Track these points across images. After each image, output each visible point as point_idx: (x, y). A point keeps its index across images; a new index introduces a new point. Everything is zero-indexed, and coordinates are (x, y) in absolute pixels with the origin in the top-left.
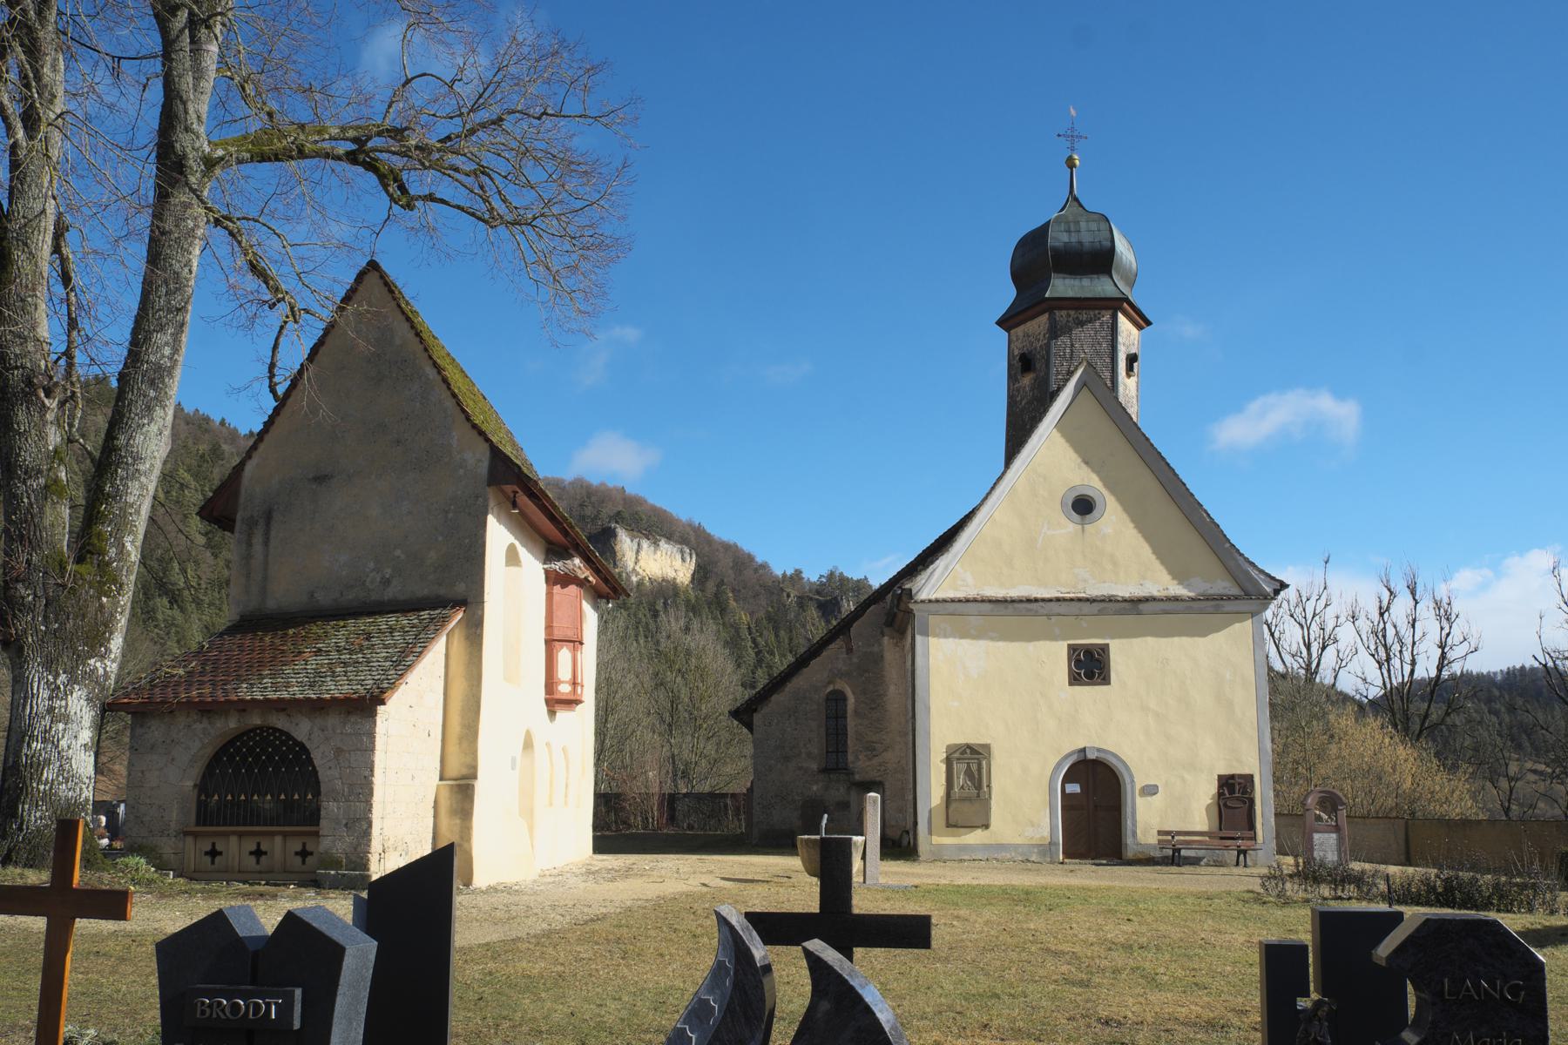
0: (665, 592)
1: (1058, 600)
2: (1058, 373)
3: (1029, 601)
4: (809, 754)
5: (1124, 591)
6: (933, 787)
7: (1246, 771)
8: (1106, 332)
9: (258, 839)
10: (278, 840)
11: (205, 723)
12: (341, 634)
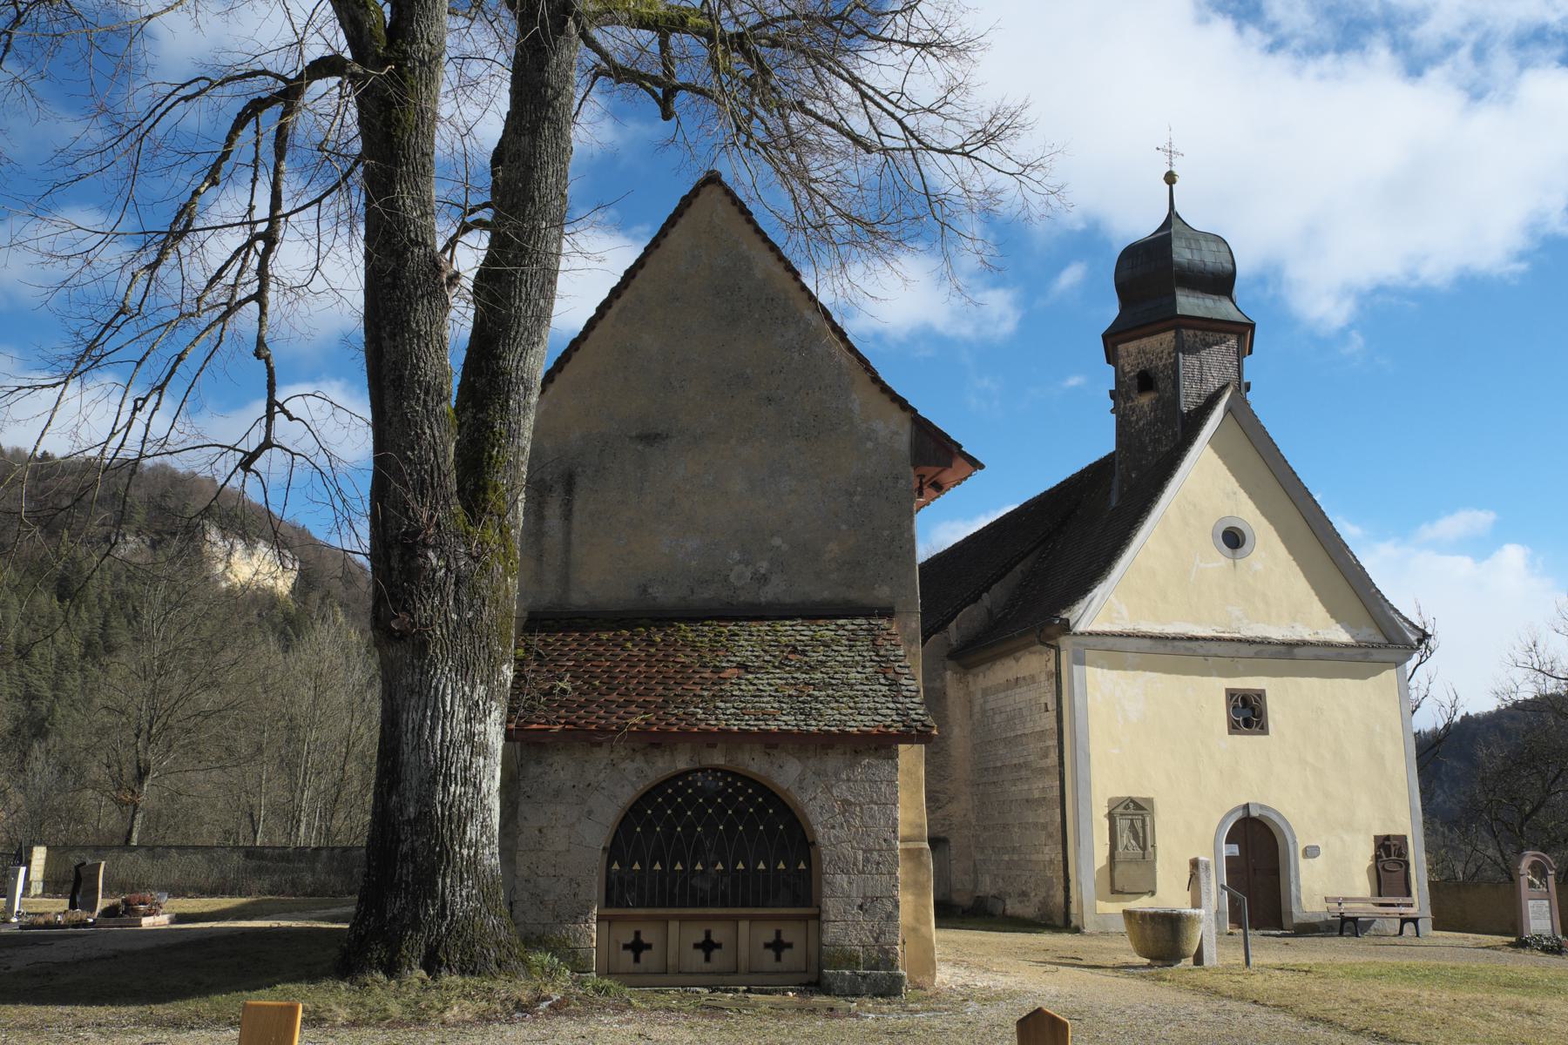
0: (259, 601)
1: (1219, 639)
2: (1187, 395)
5: (1277, 633)
6: (1094, 847)
7: (1400, 832)
11: (640, 762)
12: (749, 641)
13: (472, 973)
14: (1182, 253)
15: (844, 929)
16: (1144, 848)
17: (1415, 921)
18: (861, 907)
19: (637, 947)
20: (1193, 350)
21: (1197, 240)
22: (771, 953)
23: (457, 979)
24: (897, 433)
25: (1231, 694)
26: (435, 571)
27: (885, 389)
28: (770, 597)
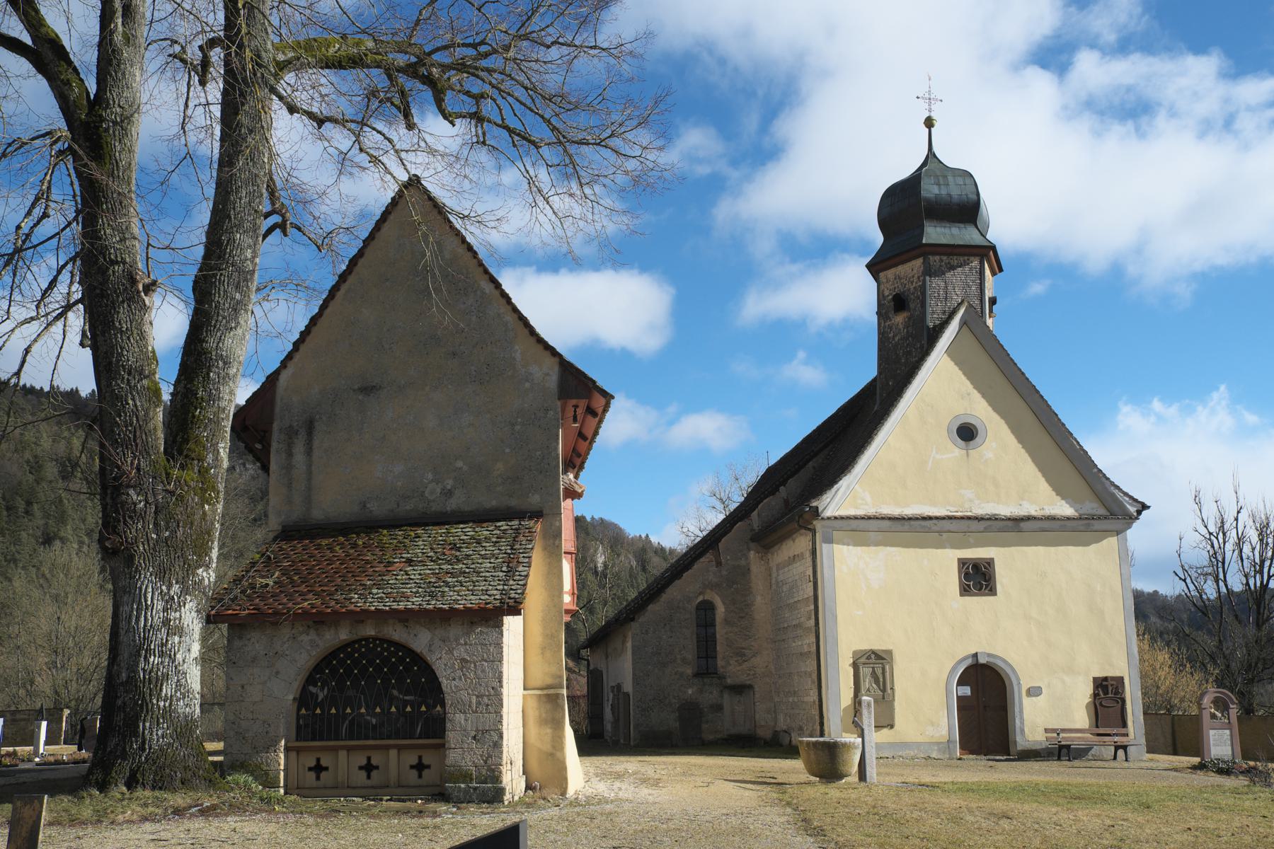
1: (950, 518)
2: (933, 313)
3: (924, 518)
4: (684, 660)
5: (1005, 510)
6: (841, 688)
7: (1118, 674)
8: (975, 276)
9: (368, 753)
10: (393, 753)
11: (312, 635)
12: (424, 542)
13: (161, 789)
14: (930, 189)
15: (461, 753)
16: (884, 690)
17: (1125, 748)
18: (474, 738)
19: (318, 769)
20: (939, 273)
21: (945, 177)
22: (415, 773)
23: (148, 793)
24: (548, 374)
25: (962, 563)
26: (135, 504)
27: (540, 340)
28: (454, 507)
